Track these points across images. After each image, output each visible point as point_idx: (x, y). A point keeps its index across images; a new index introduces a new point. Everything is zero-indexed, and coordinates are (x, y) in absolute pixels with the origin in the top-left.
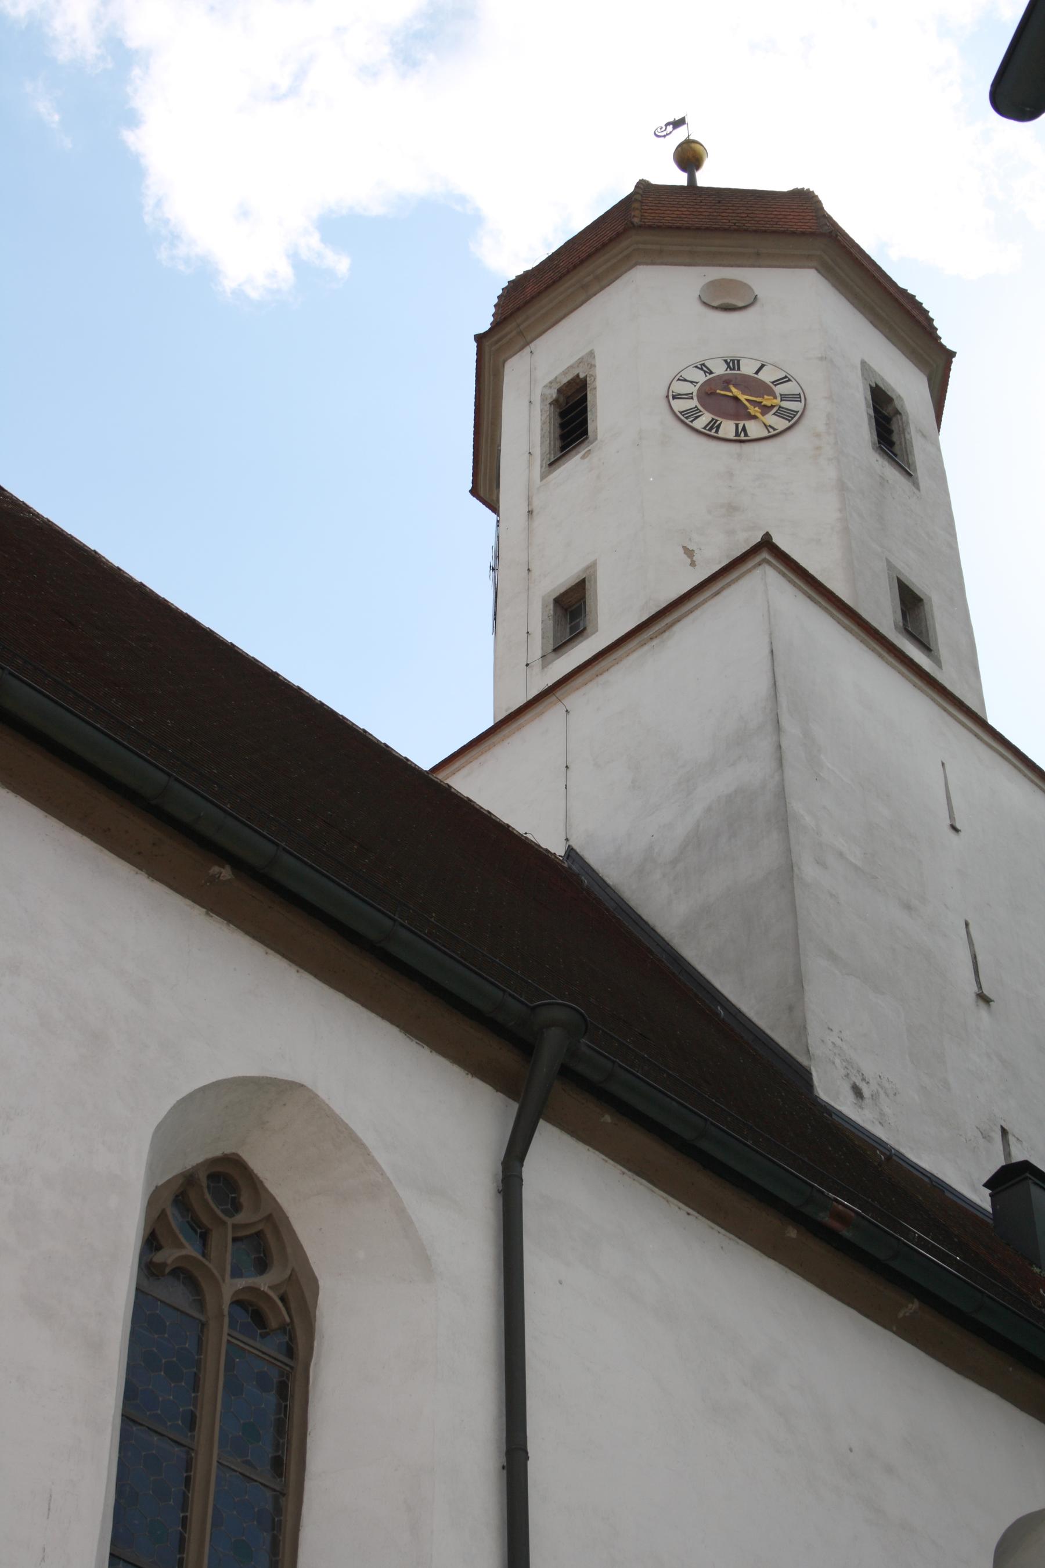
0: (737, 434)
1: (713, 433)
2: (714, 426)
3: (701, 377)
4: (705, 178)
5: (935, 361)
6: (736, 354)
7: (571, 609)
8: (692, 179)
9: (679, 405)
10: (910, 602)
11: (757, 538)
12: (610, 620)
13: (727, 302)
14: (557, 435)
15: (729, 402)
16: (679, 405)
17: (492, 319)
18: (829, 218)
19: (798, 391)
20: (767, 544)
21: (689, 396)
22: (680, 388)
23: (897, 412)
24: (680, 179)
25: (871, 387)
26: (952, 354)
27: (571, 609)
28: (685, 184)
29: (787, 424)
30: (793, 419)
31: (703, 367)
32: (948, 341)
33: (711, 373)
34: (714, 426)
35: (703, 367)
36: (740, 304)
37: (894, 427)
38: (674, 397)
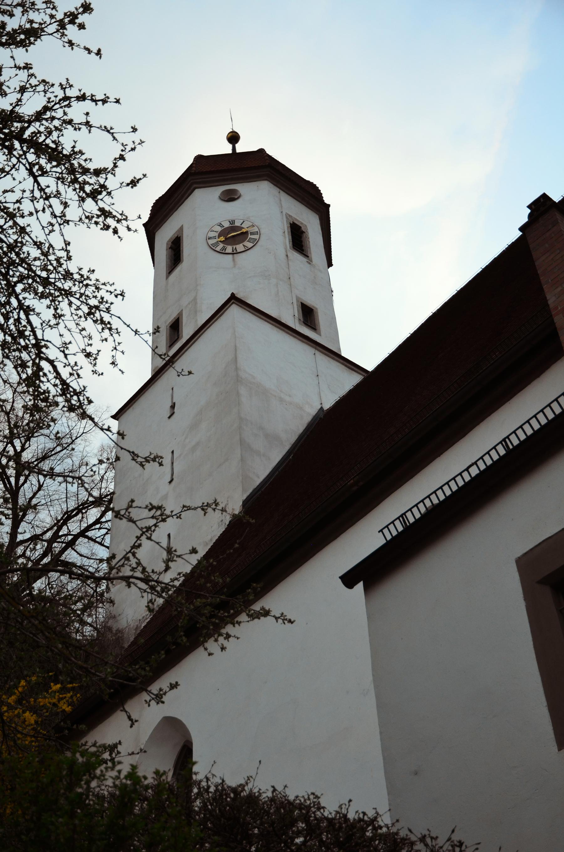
0: (233, 251)
1: (223, 252)
2: (224, 249)
3: (219, 229)
4: (241, 148)
5: (322, 210)
6: (233, 218)
7: (175, 327)
8: (234, 149)
9: (211, 242)
10: (308, 314)
11: (229, 295)
12: (187, 332)
13: (230, 197)
14: (306, 233)
15: (234, 237)
16: (211, 242)
17: (149, 216)
18: (270, 157)
19: (257, 230)
20: (233, 299)
21: (214, 238)
22: (212, 234)
23: (303, 232)
24: (227, 149)
25: (290, 224)
26: (329, 206)
27: (175, 327)
28: (230, 152)
29: (252, 245)
30: (255, 242)
31: (220, 225)
32: (327, 201)
33: (223, 227)
34: (224, 249)
35: (220, 225)
36: (236, 197)
37: (303, 239)
38: (209, 239)
